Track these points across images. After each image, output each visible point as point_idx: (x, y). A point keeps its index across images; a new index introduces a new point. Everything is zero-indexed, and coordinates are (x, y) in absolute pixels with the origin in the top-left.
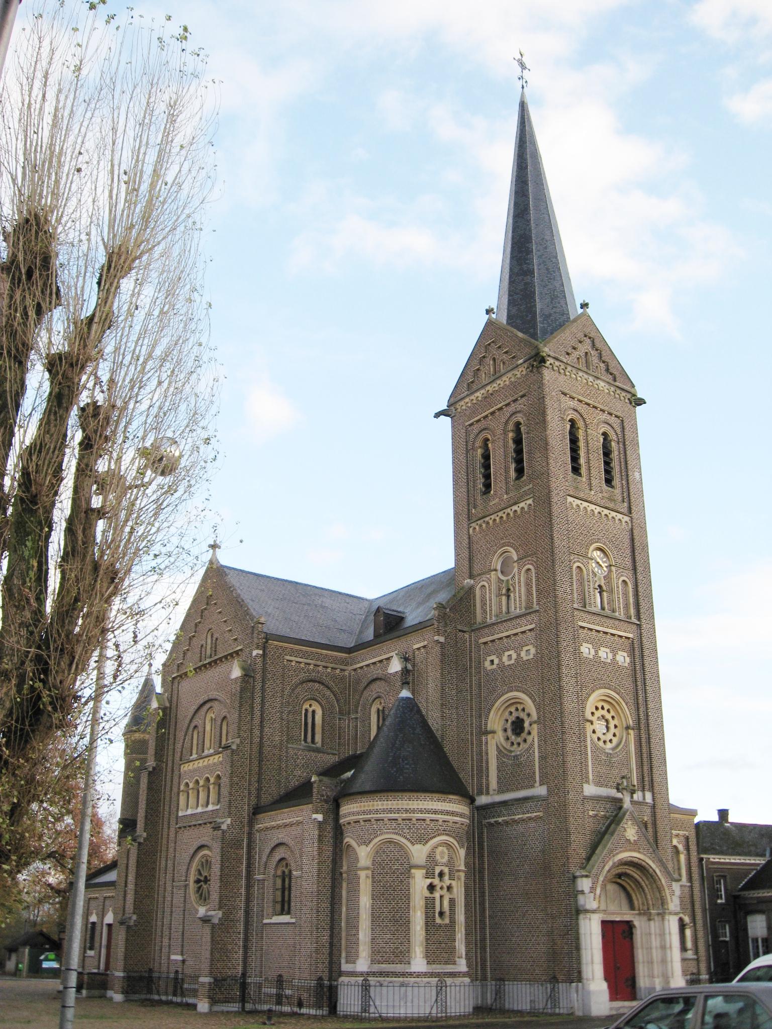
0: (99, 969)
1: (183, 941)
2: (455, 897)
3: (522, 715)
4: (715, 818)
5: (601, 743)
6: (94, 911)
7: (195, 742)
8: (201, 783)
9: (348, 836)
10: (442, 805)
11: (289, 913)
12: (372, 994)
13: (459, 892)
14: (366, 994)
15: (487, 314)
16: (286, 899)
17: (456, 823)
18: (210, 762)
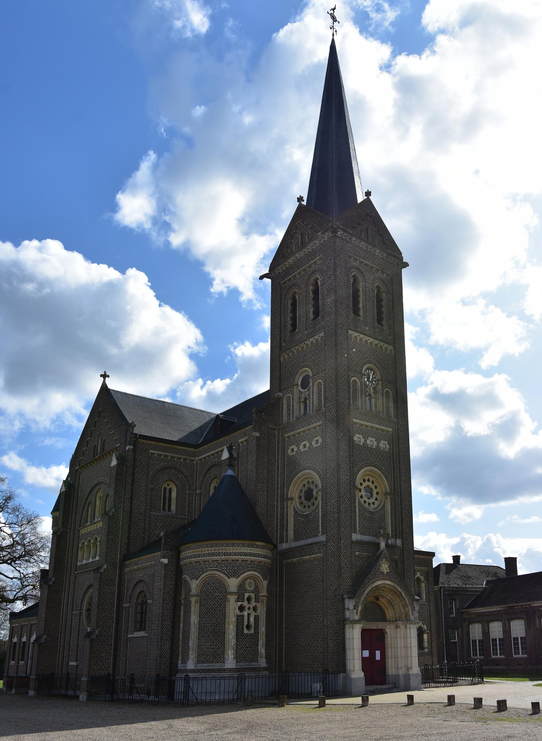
0: (26, 673)
1: (77, 652)
2: (259, 614)
3: (313, 487)
4: (451, 561)
5: (366, 505)
6: (25, 634)
7: (89, 514)
8: (92, 541)
9: (185, 574)
10: (250, 550)
11: (144, 630)
12: (191, 685)
13: (262, 611)
14: (187, 686)
15: (298, 201)
16: (143, 620)
17: (261, 562)
18: (98, 527)
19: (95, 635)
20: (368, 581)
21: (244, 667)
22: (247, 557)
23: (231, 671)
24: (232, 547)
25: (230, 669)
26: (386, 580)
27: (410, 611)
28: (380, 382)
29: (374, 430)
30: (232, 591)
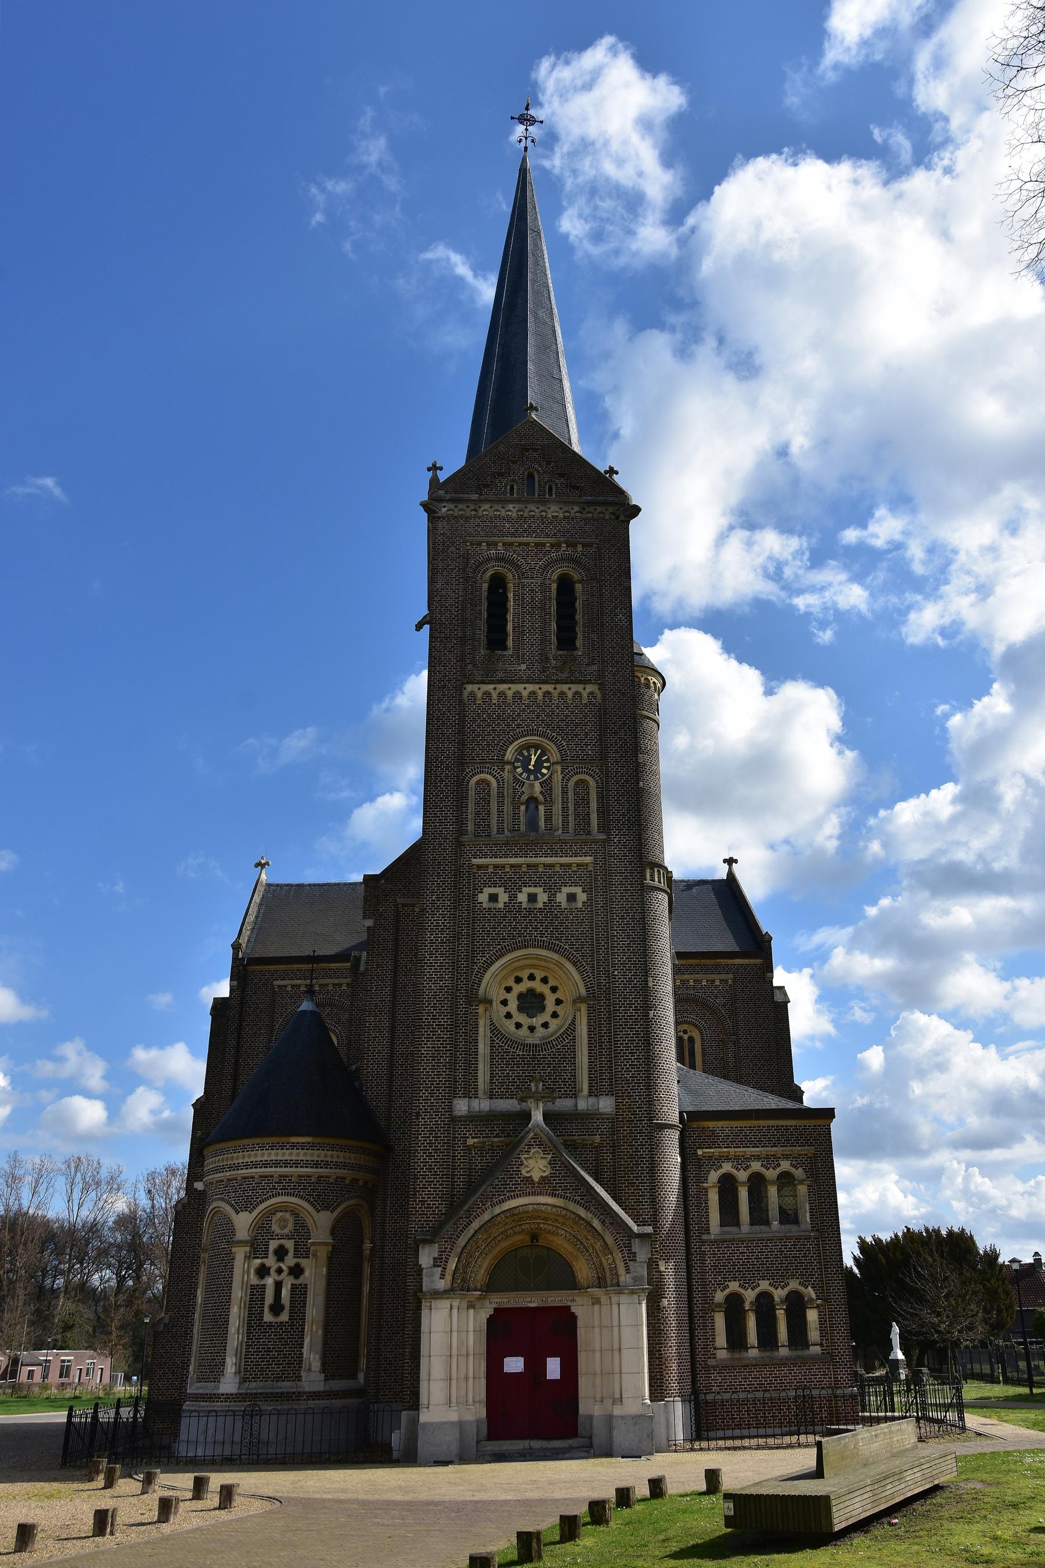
20: (482, 1201)
21: (255, 1391)
22: (269, 1169)
23: (229, 1398)
26: (540, 1194)
27: (618, 1262)
28: (559, 768)
29: (541, 870)
30: (241, 1238)
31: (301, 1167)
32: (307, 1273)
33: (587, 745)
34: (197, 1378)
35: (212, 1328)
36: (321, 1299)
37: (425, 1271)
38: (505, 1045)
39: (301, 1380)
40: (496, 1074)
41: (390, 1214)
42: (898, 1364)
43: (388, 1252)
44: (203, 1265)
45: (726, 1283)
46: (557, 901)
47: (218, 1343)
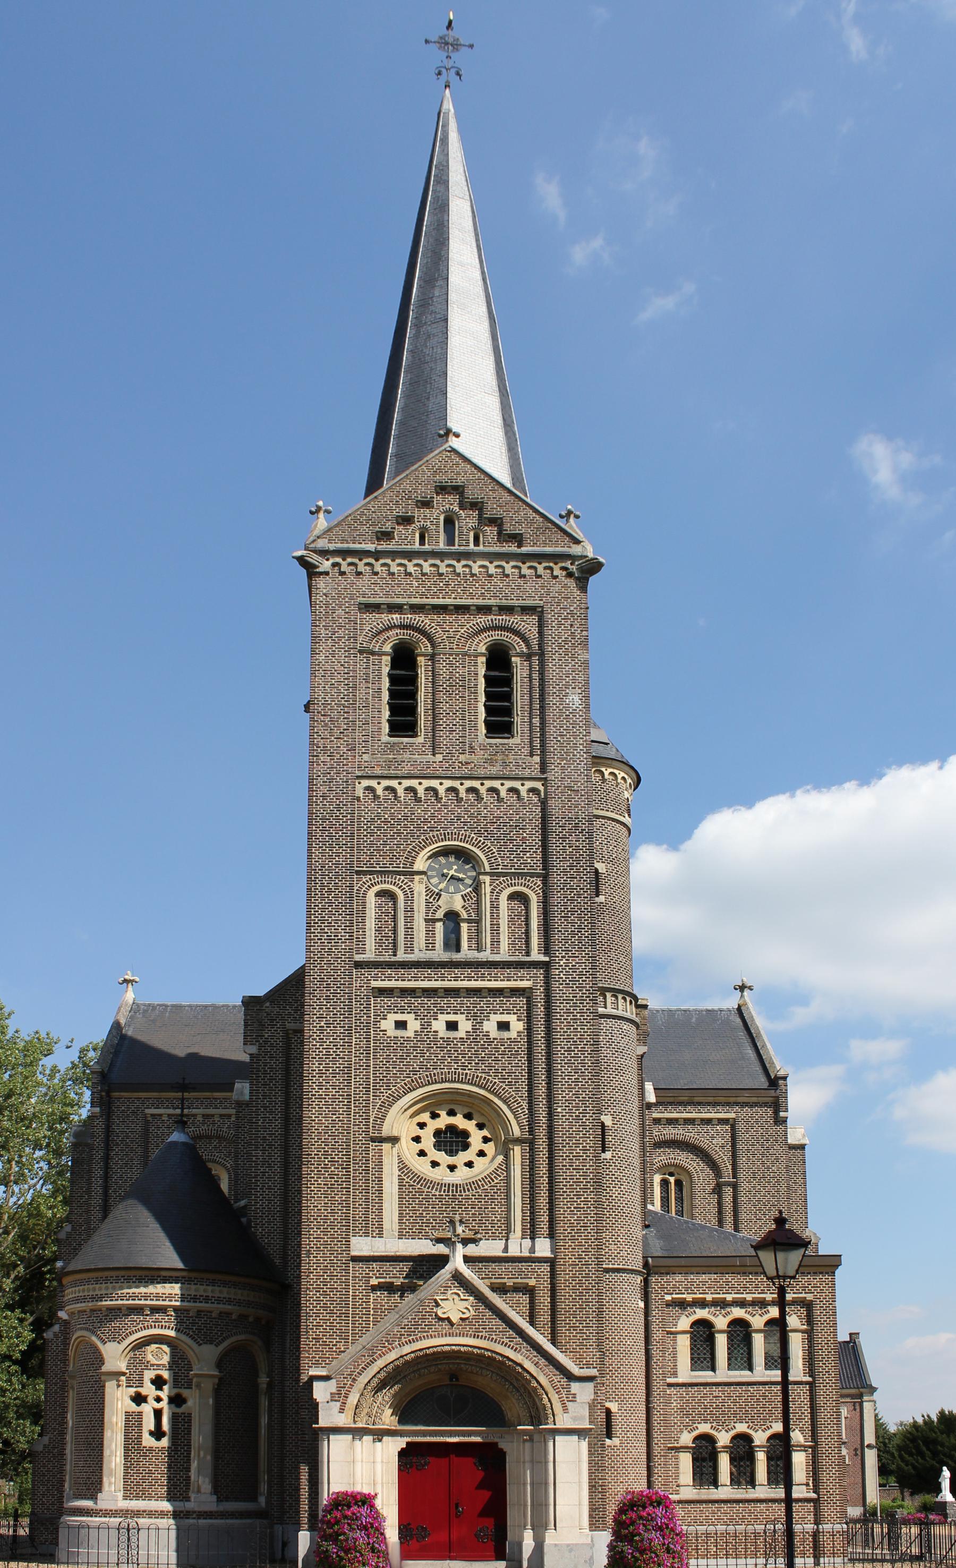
19: (42, 1446)
23: (109, 1514)
24: (105, 1283)
25: (107, 1510)
31: (150, 1300)
32: (190, 1403)
33: (524, 852)
34: (74, 1495)
35: (85, 1450)
36: (208, 1428)
37: (320, 1405)
38: (418, 1184)
39: (189, 1501)
40: (406, 1214)
41: (291, 1351)
42: (169, 1492)
43: (289, 1386)
44: (71, 1392)
45: (695, 1425)
46: (484, 1030)
47: (93, 1464)
